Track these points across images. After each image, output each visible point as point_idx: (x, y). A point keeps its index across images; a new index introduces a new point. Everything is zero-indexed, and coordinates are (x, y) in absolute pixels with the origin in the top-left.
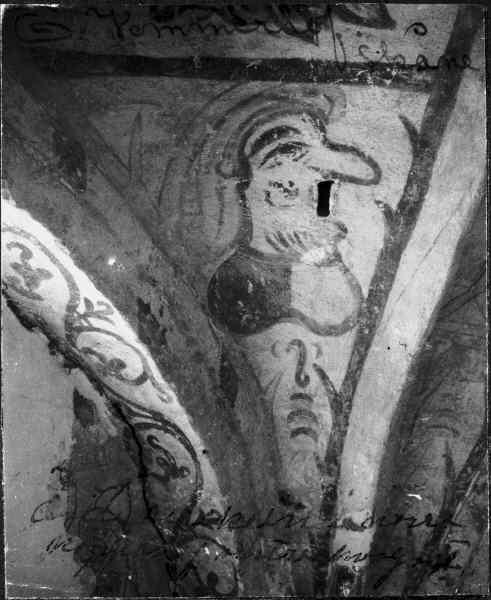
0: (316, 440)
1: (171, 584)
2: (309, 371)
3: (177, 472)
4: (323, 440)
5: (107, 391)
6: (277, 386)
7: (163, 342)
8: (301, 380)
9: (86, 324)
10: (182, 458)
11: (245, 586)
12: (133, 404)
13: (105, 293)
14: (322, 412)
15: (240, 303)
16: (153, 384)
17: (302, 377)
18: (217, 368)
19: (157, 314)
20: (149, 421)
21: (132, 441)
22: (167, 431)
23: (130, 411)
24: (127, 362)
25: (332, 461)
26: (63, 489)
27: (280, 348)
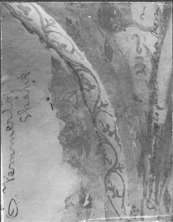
0: (146, 75)
1: (95, 128)
2: (141, 46)
3: (93, 87)
4: (149, 75)
5: (64, 57)
6: (130, 53)
7: (79, 35)
8: (139, 51)
9: (49, 30)
10: (93, 83)
11: (119, 128)
12: (74, 62)
13: (51, 15)
14: (148, 64)
15: (111, 19)
16: (77, 53)
17: (139, 50)
18: (103, 46)
19: (75, 24)
20: (80, 68)
21: (76, 76)
22: (86, 71)
23: (73, 65)
24: (67, 45)
25: (153, 82)
26: (50, 92)
27: (129, 38)
